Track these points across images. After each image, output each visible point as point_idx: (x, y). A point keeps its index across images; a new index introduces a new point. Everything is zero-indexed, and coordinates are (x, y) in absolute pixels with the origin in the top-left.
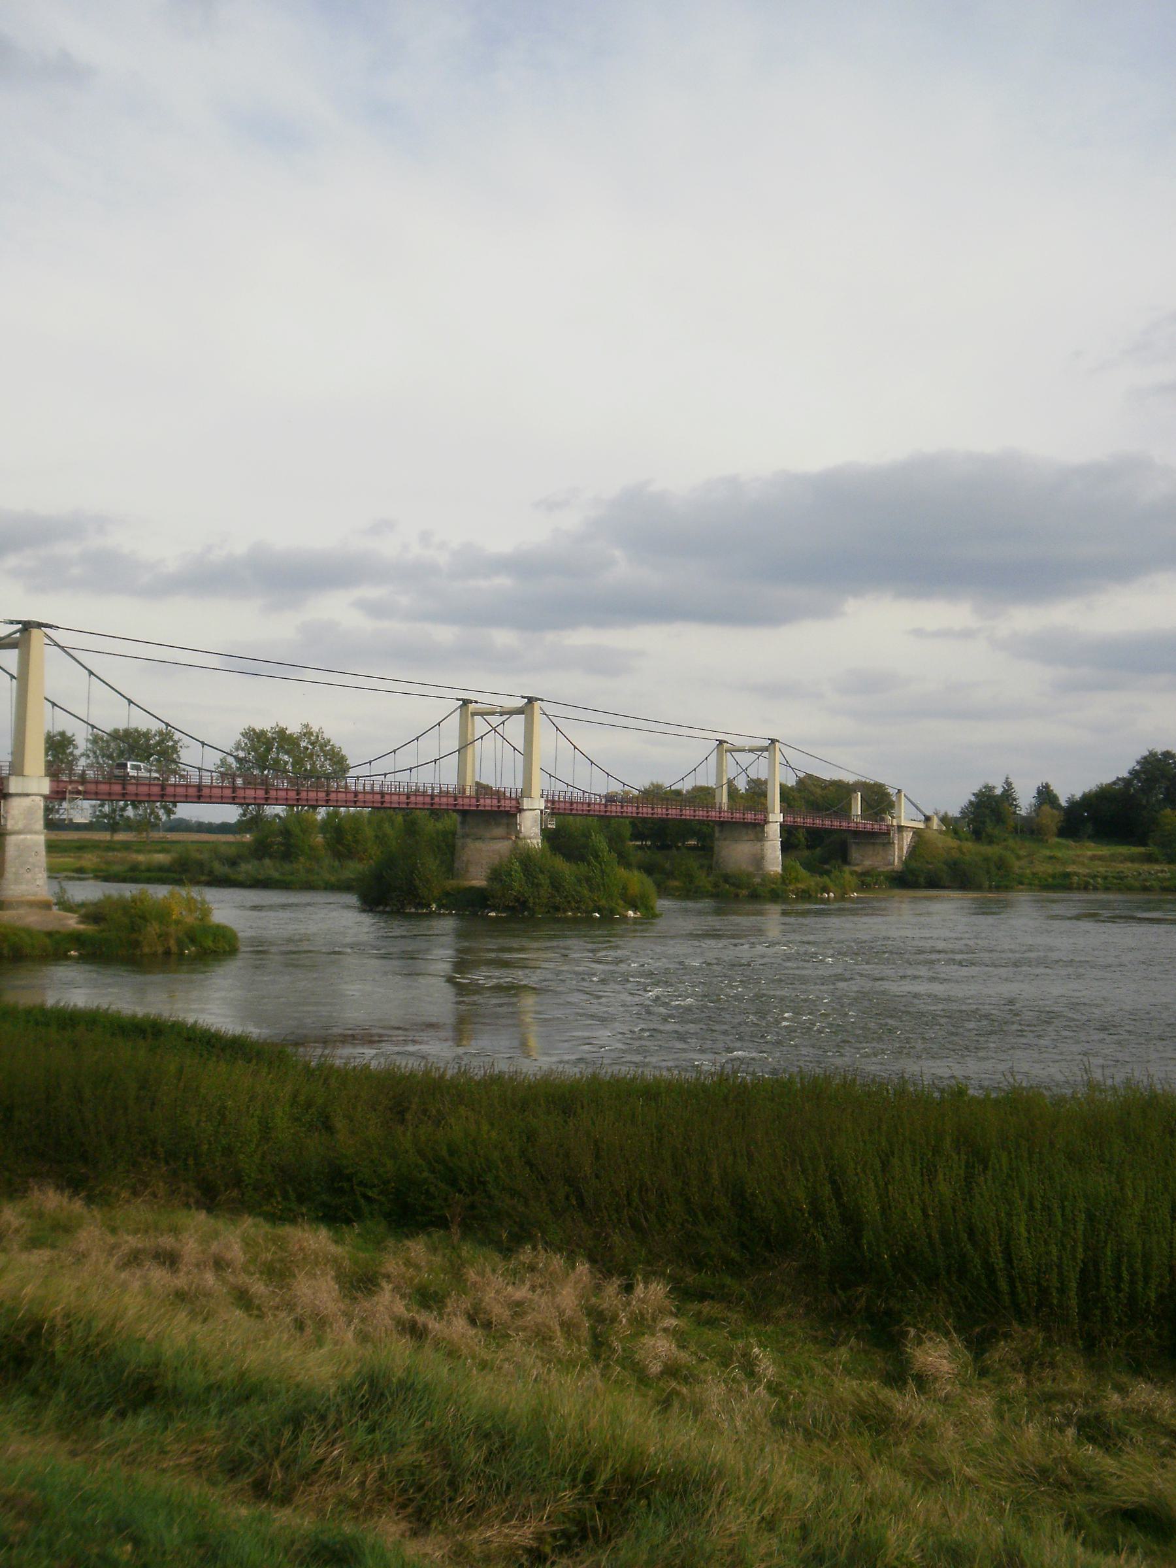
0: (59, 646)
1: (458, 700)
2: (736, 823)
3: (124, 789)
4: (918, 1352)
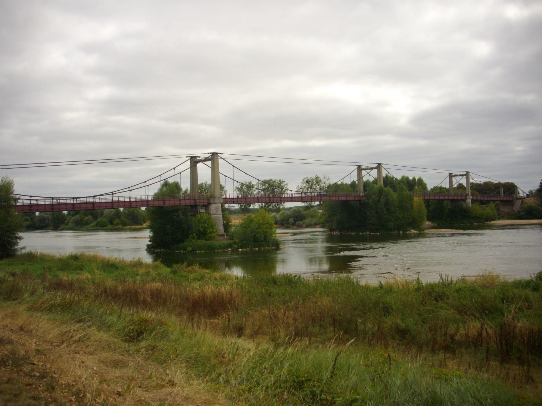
0: (222, 159)
1: (376, 164)
2: (459, 200)
3: (164, 202)
4: (173, 315)
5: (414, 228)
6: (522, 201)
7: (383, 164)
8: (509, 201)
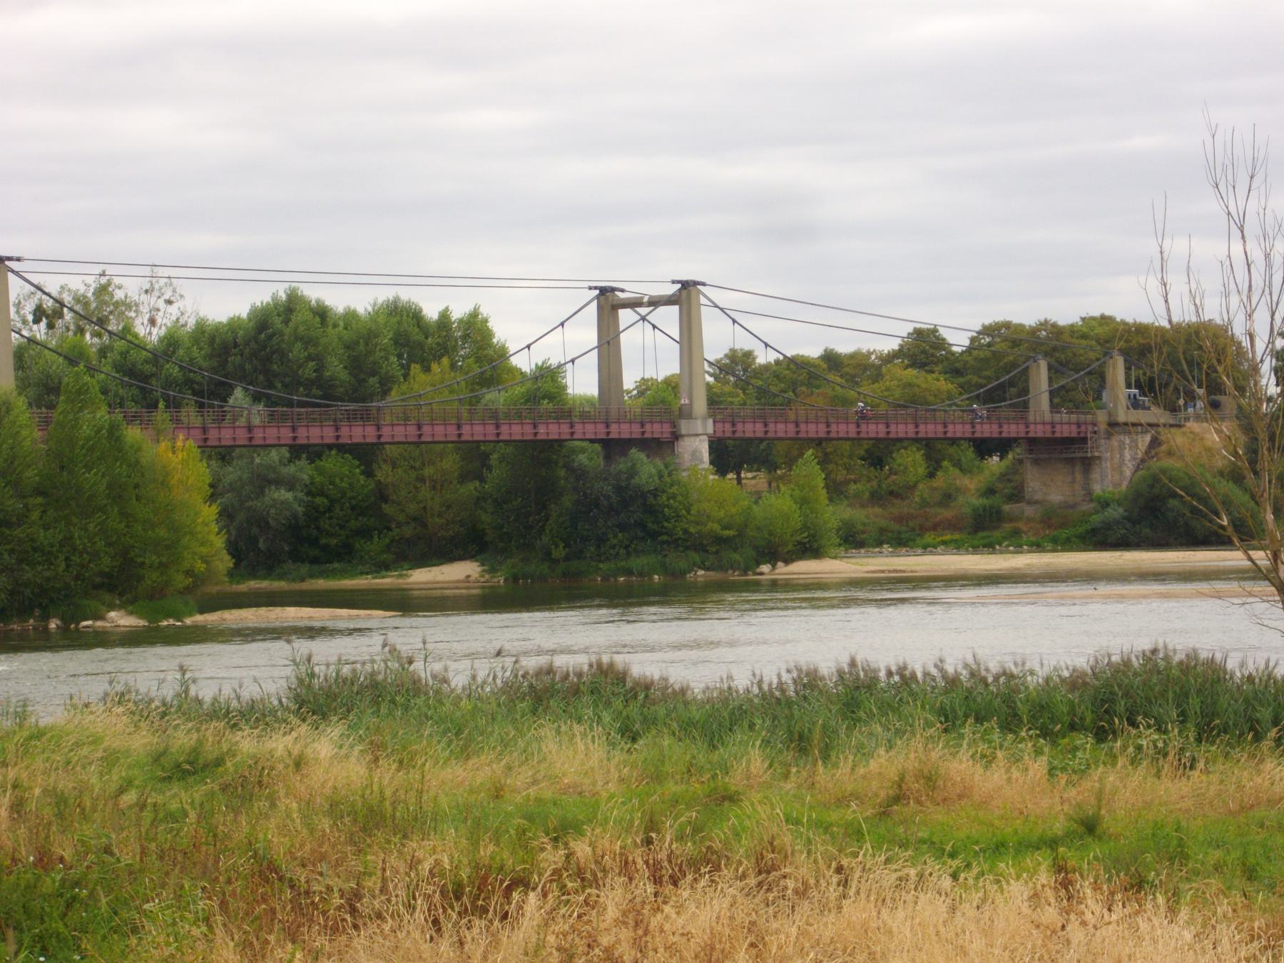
1: (674, 282)
5: (129, 605)
6: (1155, 443)
7: (704, 284)
8: (1068, 442)
